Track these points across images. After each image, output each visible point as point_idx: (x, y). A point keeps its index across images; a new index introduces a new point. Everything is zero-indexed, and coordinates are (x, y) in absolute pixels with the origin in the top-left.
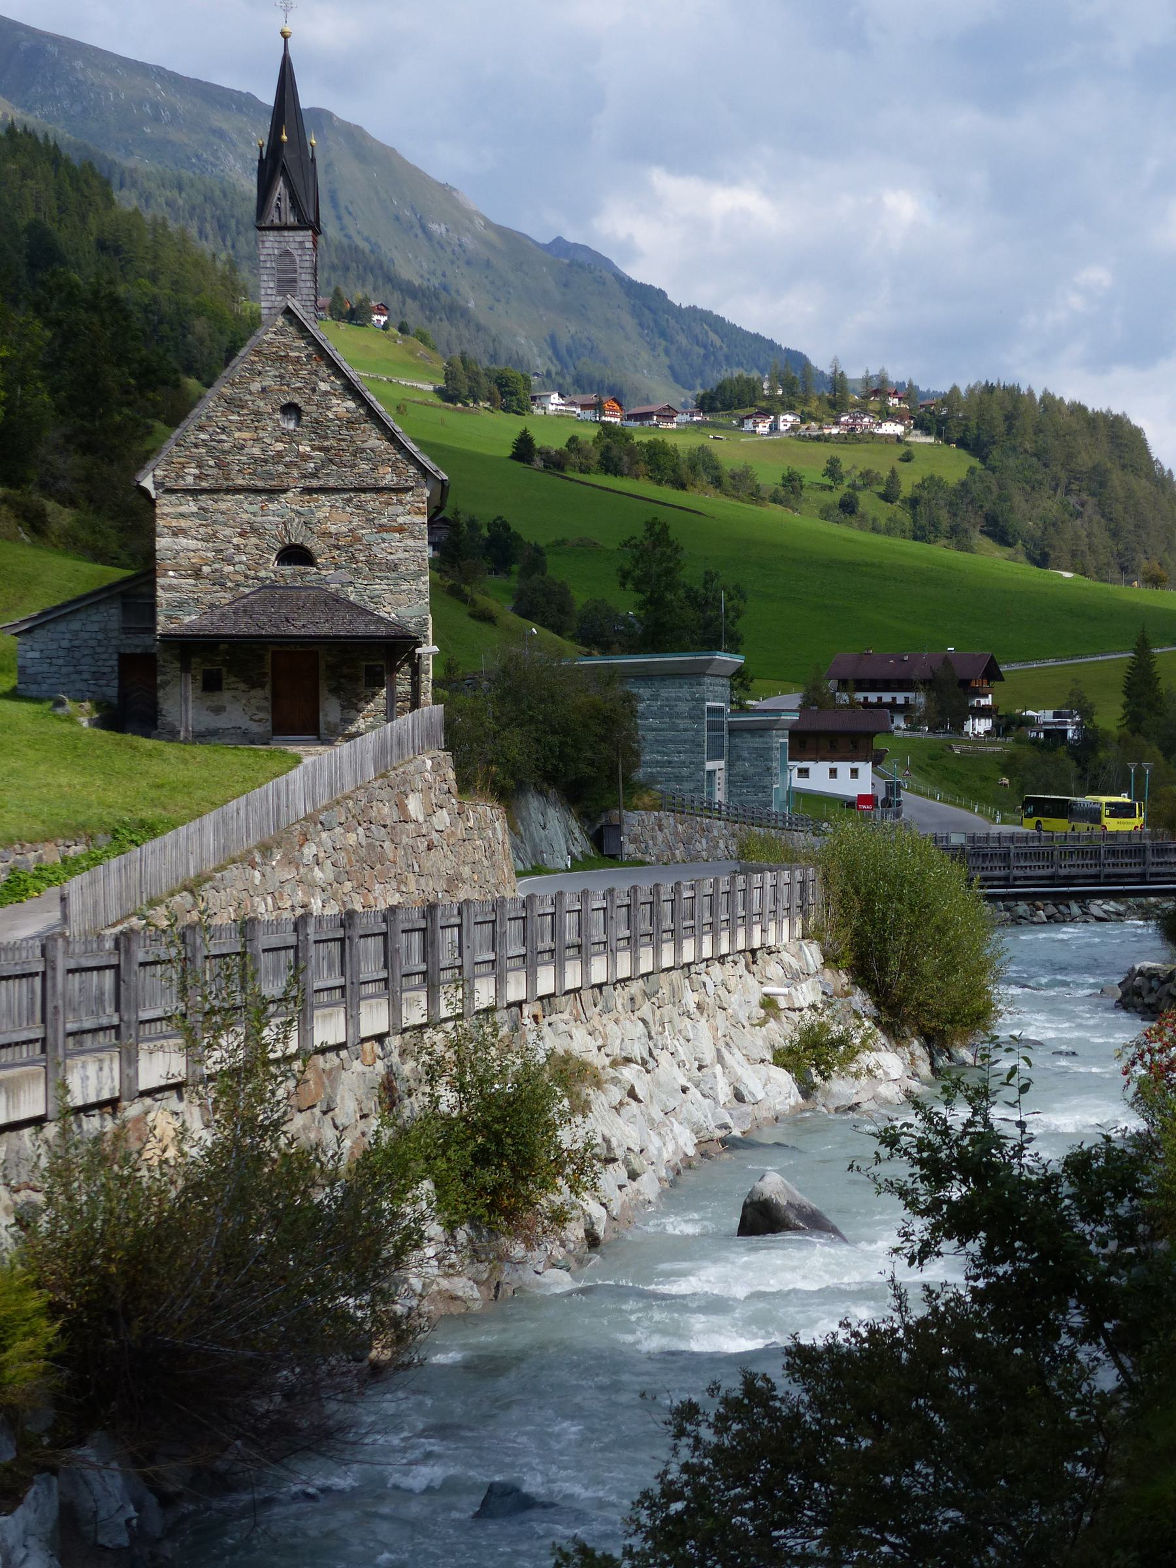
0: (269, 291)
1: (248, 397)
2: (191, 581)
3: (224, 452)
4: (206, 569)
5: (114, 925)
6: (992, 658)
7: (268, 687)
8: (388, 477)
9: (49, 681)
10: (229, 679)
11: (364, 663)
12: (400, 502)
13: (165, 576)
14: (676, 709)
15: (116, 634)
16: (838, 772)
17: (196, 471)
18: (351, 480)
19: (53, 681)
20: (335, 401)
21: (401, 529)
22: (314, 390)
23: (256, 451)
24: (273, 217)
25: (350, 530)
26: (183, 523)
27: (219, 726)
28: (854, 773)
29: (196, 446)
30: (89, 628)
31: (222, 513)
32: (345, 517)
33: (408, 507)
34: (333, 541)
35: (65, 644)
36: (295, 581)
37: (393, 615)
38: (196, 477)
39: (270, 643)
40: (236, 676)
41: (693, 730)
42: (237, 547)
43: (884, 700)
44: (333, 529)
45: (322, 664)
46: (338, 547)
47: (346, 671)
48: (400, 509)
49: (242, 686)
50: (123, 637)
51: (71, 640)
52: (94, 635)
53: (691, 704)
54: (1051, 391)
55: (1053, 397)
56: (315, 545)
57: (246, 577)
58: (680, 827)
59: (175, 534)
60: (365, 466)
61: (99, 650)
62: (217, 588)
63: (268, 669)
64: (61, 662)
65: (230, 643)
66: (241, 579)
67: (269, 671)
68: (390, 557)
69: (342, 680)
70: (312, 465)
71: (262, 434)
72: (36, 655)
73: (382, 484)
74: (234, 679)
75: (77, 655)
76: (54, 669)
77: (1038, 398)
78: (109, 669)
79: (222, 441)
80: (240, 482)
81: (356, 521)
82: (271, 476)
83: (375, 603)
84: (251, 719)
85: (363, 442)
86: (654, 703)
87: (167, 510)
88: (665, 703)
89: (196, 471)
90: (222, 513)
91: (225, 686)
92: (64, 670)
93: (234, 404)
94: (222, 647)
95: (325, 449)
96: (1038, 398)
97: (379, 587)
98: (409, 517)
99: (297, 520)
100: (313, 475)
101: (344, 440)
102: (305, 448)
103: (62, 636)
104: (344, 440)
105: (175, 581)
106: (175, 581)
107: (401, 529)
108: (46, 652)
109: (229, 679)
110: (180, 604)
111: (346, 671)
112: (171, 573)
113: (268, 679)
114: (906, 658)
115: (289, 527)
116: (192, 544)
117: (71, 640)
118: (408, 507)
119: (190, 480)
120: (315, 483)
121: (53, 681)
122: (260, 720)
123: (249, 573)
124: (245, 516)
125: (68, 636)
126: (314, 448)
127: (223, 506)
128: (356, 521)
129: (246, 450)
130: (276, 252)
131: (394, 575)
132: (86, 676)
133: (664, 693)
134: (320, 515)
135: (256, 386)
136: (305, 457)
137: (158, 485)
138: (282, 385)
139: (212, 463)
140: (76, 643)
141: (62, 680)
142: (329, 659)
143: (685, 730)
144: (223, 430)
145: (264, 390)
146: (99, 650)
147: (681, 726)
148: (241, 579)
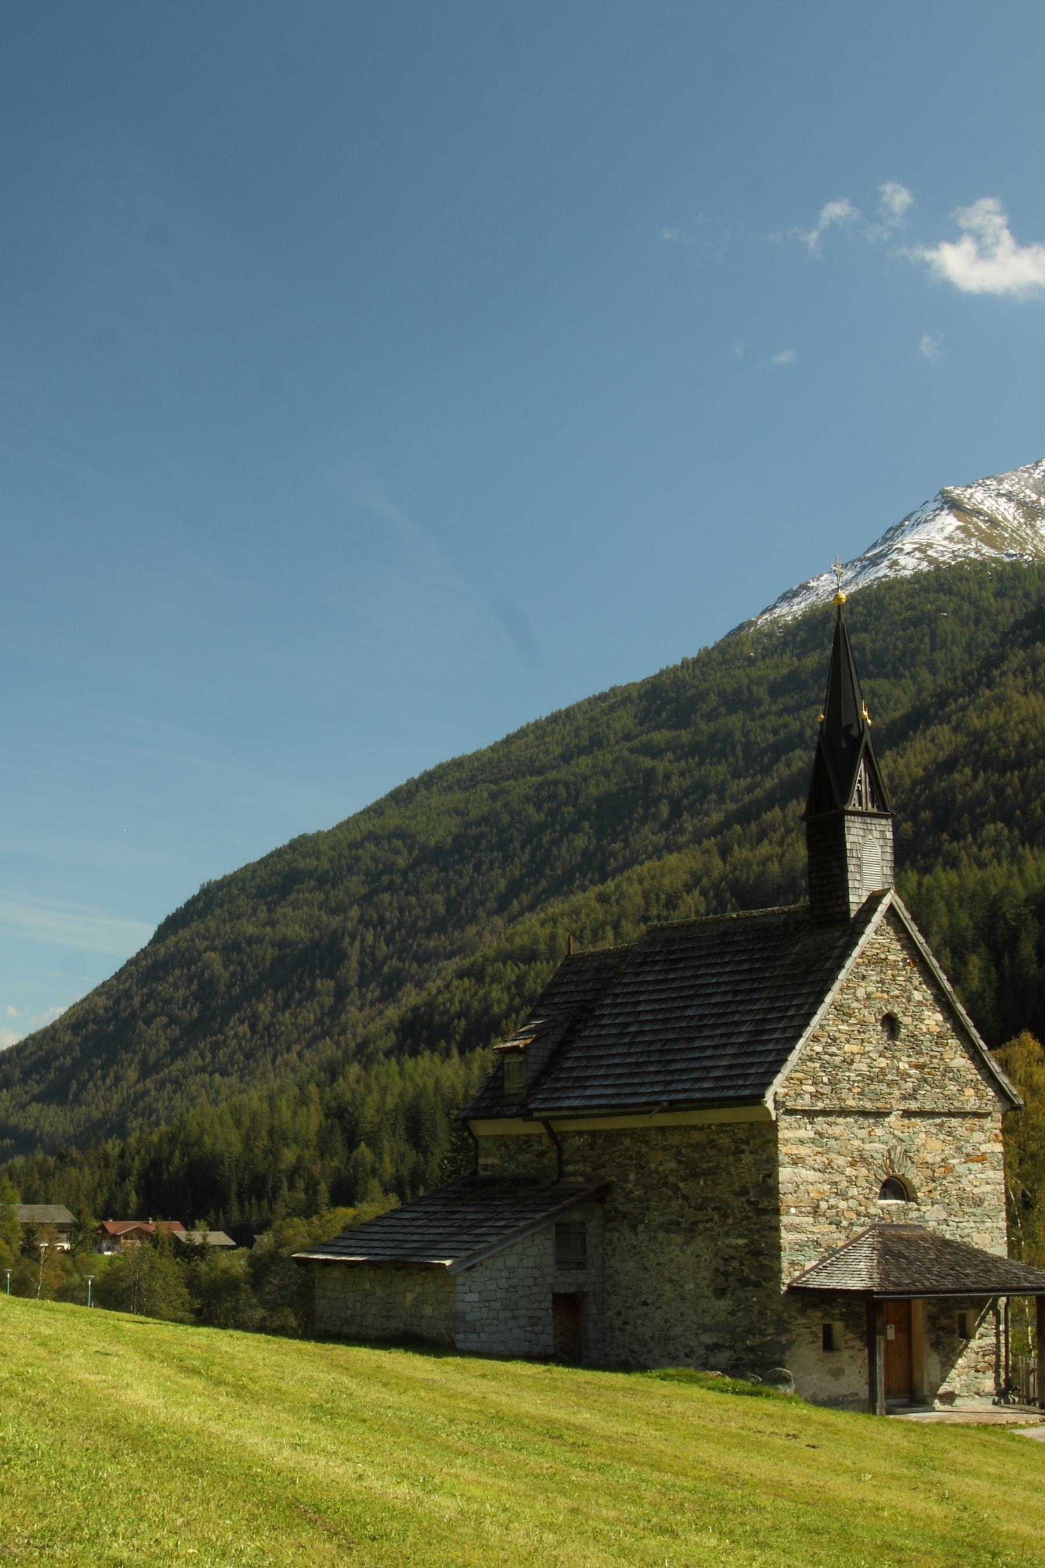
1: (855, 1005)
4: (823, 1205)
13: (788, 1213)
18: (943, 1106)
22: (909, 1000)
26: (803, 1151)
47: (944, 1322)
64: (498, 1305)
66: (854, 1216)
68: (976, 1191)
74: (850, 1336)
80: (851, 1102)
89: (812, 1089)
92: (502, 1315)
99: (899, 1148)
100: (912, 1096)
120: (913, 1106)
125: (505, 1274)
127: (836, 1131)
129: (855, 1066)
136: (904, 1076)
140: (514, 1282)
146: (535, 1289)
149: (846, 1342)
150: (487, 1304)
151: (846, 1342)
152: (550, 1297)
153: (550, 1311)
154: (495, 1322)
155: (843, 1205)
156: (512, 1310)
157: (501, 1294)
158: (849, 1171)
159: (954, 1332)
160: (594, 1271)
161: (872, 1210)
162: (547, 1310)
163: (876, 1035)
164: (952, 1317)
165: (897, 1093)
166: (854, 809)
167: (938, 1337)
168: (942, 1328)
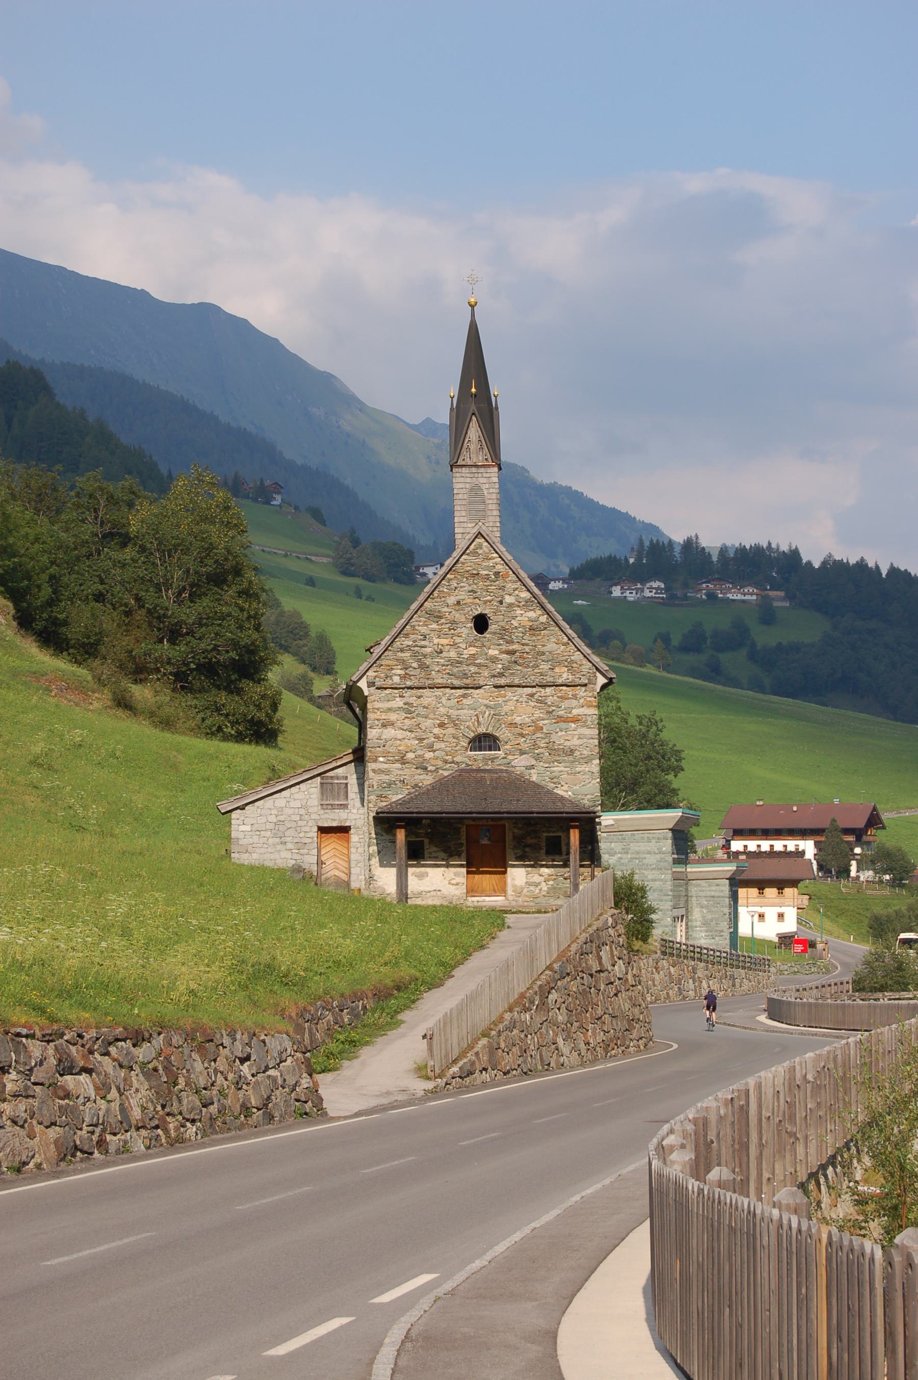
0: (462, 519)
1: (445, 609)
2: (398, 765)
3: (425, 656)
4: (410, 756)
5: (455, 1062)
6: (875, 809)
7: (464, 855)
8: (565, 676)
9: (258, 850)
10: (429, 849)
11: (545, 834)
12: (575, 697)
13: (375, 761)
14: (646, 861)
15: (315, 809)
16: (785, 916)
17: (402, 672)
18: (534, 679)
19: (263, 850)
20: (519, 612)
21: (575, 720)
22: (501, 602)
23: (453, 654)
24: (466, 458)
25: (533, 721)
26: (393, 717)
27: (422, 889)
28: (781, 916)
29: (402, 651)
30: (292, 804)
31: (424, 707)
32: (529, 709)
33: (582, 701)
34: (518, 730)
35: (273, 819)
36: (487, 764)
37: (570, 793)
38: (403, 677)
39: (465, 818)
40: (436, 846)
41: (662, 880)
42: (437, 737)
43: (776, 849)
44: (518, 720)
45: (509, 837)
46: (522, 735)
47: (530, 841)
48: (574, 703)
49: (442, 855)
50: (322, 812)
51: (277, 816)
52: (296, 810)
53: (658, 857)
54: (895, 565)
55: (898, 570)
56: (503, 734)
57: (446, 762)
58: (672, 969)
59: (384, 726)
60: (545, 667)
61: (300, 823)
62: (419, 771)
63: (463, 840)
64: (268, 834)
65: (432, 819)
66: (440, 763)
67: (464, 842)
68: (568, 743)
69: (527, 849)
70: (500, 666)
71: (458, 640)
72: (248, 828)
73: (560, 681)
74: (434, 849)
75: (282, 828)
76: (261, 841)
77: (884, 573)
78: (310, 840)
79: (425, 647)
80: (440, 681)
81: (538, 714)
82: (465, 676)
83: (555, 783)
84: (450, 883)
85: (544, 646)
86: (624, 856)
87: (377, 705)
88: (634, 856)
89: (402, 672)
90: (424, 707)
91: (426, 855)
92: (271, 841)
93: (436, 616)
94: (424, 821)
95: (512, 653)
96: (884, 573)
97: (557, 768)
98: (582, 709)
99: (487, 713)
100: (501, 675)
101: (527, 645)
102: (493, 652)
103: (269, 812)
104: (527, 645)
105: (386, 766)
106: (386, 766)
107: (575, 720)
108: (256, 826)
109: (429, 849)
110: (390, 785)
111: (530, 841)
112: (381, 759)
113: (464, 848)
114: (795, 809)
115: (481, 719)
116: (400, 734)
117: (277, 816)
118: (582, 701)
119: (396, 679)
120: (502, 681)
121: (263, 850)
122: (457, 884)
123: (447, 758)
124: (442, 710)
125: (274, 812)
126: (502, 652)
127: (425, 701)
128: (538, 714)
129: (444, 654)
130: (468, 486)
131: (571, 758)
132: (289, 846)
133: (634, 847)
134: (506, 709)
135: (452, 600)
136: (494, 660)
137: (371, 684)
138: (475, 598)
139: (415, 665)
140: (282, 818)
141: (269, 850)
142: (516, 831)
143: (654, 880)
144: (425, 637)
145: (458, 603)
146: (300, 823)
147: (650, 877)
148: (440, 763)
149: (431, 853)
150: (258, 833)
151: (431, 853)
152: (316, 829)
153: (315, 839)
154: (266, 846)
155: (429, 755)
156: (281, 837)
157: (271, 826)
158: (436, 731)
159: (541, 848)
160: (355, 811)
161: (458, 759)
162: (312, 838)
163: (467, 629)
164: (539, 838)
165: (486, 673)
166: (464, 463)
167: (525, 852)
168: (530, 846)
